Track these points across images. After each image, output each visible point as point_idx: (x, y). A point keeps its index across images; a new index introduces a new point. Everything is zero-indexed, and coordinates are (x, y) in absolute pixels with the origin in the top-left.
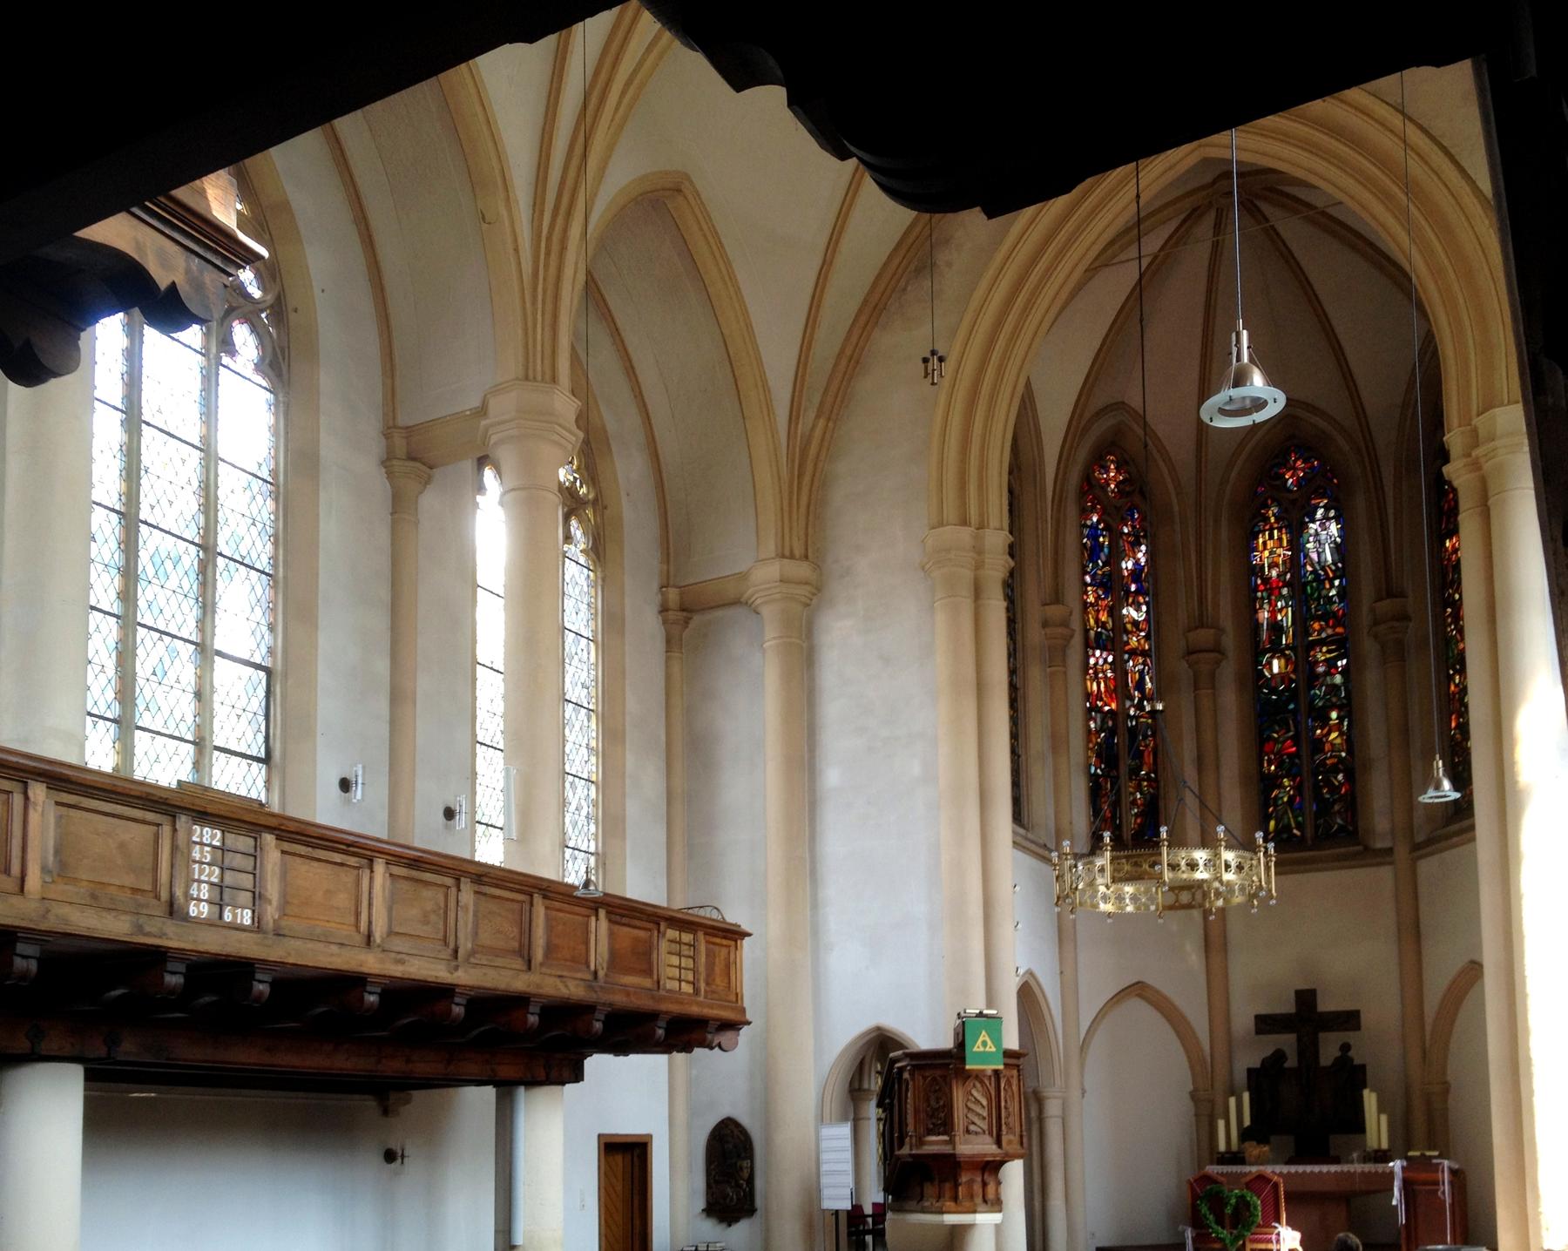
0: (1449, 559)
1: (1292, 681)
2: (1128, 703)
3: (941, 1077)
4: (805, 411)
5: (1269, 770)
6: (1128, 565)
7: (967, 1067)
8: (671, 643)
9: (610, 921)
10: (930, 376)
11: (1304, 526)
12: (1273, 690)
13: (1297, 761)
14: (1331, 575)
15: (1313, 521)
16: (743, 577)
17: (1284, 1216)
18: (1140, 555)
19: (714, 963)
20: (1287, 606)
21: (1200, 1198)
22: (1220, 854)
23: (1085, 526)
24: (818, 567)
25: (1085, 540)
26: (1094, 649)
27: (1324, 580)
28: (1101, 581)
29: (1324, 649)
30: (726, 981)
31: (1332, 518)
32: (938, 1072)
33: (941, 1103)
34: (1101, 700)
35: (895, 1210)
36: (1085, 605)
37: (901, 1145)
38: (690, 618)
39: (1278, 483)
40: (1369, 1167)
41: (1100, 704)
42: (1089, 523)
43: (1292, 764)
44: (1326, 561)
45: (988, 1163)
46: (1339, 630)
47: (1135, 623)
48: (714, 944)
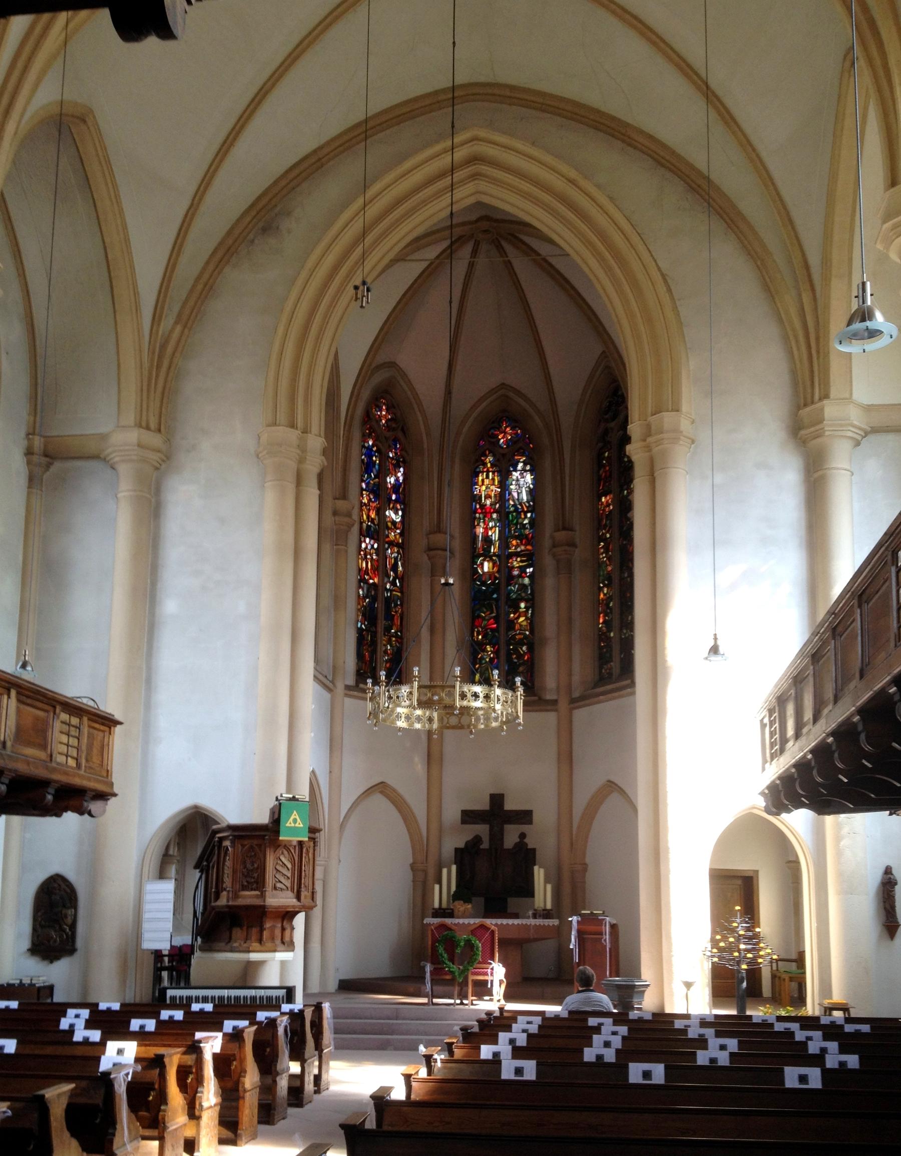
0: (604, 510)
1: (496, 578)
2: (386, 580)
3: (256, 845)
4: (166, 317)
5: (478, 638)
6: (391, 480)
7: (281, 838)
8: (32, 481)
9: (19, 701)
10: (359, 302)
11: (509, 473)
12: (484, 583)
13: (497, 634)
14: (525, 509)
15: (516, 470)
16: (104, 437)
17: (497, 955)
18: (399, 474)
19: (93, 744)
20: (495, 526)
21: (438, 941)
22: (494, 690)
23: (363, 446)
24: (168, 441)
25: (363, 457)
26: (365, 537)
27: (521, 512)
28: (373, 489)
29: (519, 559)
30: (100, 759)
31: (528, 471)
32: (255, 842)
33: (256, 866)
34: (368, 574)
35: (202, 949)
36: (362, 504)
37: (217, 897)
38: (51, 464)
39: (493, 440)
40: (539, 922)
41: (366, 577)
42: (366, 445)
43: (494, 636)
44: (522, 499)
45: (288, 912)
46: (529, 547)
47: (394, 523)
48: (95, 728)
